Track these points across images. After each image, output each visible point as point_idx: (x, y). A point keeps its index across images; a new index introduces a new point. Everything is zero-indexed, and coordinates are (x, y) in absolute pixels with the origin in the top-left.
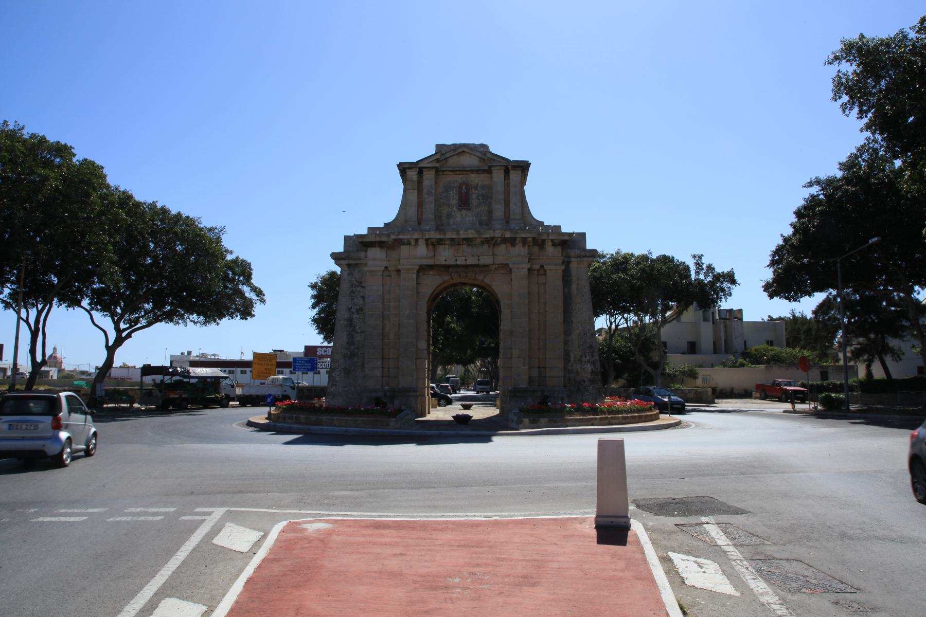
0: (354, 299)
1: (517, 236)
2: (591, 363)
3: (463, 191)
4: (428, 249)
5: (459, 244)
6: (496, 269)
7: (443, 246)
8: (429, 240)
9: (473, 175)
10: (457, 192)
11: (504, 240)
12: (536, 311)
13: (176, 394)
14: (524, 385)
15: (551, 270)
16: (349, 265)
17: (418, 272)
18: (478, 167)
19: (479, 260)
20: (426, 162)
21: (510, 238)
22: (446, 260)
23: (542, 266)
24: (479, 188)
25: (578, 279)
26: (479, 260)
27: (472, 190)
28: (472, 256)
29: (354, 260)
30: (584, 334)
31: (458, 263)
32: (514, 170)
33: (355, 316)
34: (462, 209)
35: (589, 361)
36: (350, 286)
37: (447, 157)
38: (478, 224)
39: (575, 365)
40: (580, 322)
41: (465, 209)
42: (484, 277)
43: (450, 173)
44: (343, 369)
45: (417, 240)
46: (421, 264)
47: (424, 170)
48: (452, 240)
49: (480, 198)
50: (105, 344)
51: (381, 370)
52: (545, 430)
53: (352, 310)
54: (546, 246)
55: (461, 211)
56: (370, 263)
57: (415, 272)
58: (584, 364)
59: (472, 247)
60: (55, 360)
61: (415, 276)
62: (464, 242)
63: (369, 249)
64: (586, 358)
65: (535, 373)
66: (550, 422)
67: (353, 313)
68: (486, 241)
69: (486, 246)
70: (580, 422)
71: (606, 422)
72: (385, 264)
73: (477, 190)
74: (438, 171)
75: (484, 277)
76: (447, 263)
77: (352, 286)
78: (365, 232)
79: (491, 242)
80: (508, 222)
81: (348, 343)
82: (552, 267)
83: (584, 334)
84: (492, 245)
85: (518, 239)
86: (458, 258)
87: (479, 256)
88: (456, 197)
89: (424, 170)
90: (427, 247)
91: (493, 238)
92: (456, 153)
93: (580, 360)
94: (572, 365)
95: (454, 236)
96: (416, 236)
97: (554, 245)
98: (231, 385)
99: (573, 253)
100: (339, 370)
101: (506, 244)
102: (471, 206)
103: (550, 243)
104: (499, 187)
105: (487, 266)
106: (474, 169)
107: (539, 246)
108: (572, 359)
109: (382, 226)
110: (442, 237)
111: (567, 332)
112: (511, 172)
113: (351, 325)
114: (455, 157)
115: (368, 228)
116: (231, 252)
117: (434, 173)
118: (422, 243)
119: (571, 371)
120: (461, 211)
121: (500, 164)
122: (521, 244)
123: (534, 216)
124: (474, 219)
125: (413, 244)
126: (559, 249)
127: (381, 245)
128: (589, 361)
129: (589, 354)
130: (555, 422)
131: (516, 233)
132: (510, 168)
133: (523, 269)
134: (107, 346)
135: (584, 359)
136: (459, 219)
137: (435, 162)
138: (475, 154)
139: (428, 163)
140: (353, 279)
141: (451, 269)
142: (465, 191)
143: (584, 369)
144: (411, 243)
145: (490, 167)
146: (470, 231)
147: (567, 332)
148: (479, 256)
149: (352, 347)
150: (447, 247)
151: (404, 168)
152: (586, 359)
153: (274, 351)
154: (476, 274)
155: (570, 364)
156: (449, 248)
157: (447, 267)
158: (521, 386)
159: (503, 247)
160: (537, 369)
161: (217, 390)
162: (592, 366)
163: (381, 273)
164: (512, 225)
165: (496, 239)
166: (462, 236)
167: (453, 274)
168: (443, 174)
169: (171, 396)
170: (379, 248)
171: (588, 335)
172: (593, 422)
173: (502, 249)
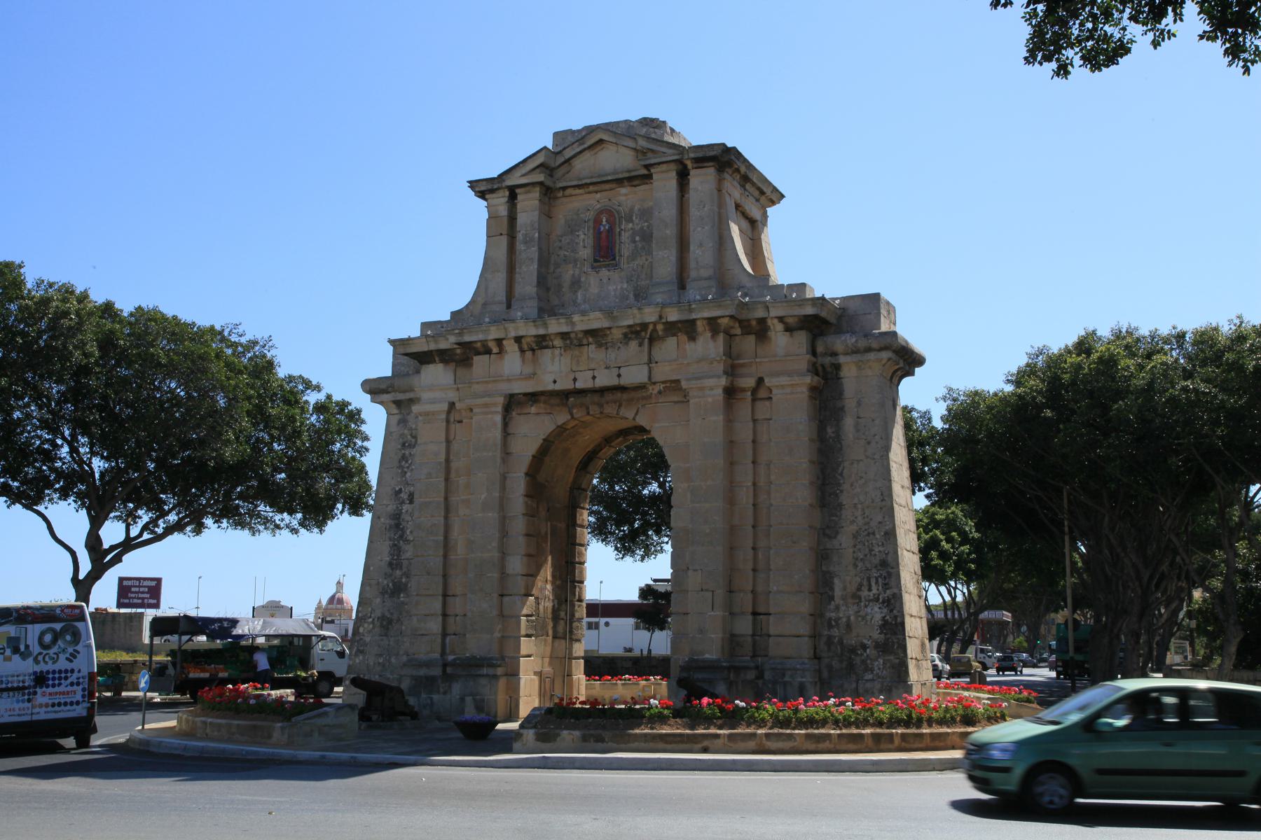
0: (406, 473)
1: (694, 316)
2: (883, 602)
3: (602, 229)
4: (523, 361)
5: (581, 345)
6: (660, 392)
8: (523, 340)
9: (623, 190)
10: (591, 231)
11: (672, 328)
12: (750, 484)
13: (203, 671)
14: (712, 652)
15: (783, 387)
16: (398, 403)
17: (507, 409)
18: (629, 171)
19: (619, 376)
20: (518, 173)
22: (555, 382)
23: (760, 381)
25: (859, 404)
26: (619, 376)
27: (620, 224)
28: (607, 368)
29: (404, 392)
30: (868, 534)
31: (579, 385)
32: (696, 168)
33: (406, 507)
34: (600, 267)
35: (877, 600)
36: (399, 447)
37: (567, 157)
38: (631, 296)
39: (843, 608)
40: (860, 506)
41: (605, 266)
42: (636, 414)
43: (578, 191)
44: (378, 618)
45: (499, 342)
46: (511, 392)
48: (564, 336)
50: (71, 576)
51: (440, 618)
52: (523, 759)
53: (402, 495)
54: (771, 334)
55: (597, 272)
56: (425, 396)
57: (500, 409)
58: (866, 606)
59: (607, 349)
60: (339, 606)
61: (498, 418)
62: (591, 340)
63: (424, 366)
64: (870, 590)
65: (744, 626)
66: (585, 739)
67: (403, 502)
68: (632, 333)
69: (633, 344)
70: (667, 742)
71: (752, 744)
72: (452, 395)
74: (549, 193)
75: (636, 414)
76: (558, 387)
77: (404, 444)
78: (415, 332)
79: (643, 334)
80: (682, 286)
81: (390, 564)
82: (784, 380)
83: (868, 534)
85: (699, 323)
86: (578, 375)
87: (619, 368)
88: (590, 242)
89: (518, 191)
90: (521, 356)
92: (586, 146)
93: (856, 597)
94: (837, 608)
95: (565, 329)
96: (494, 333)
97: (789, 329)
98: (337, 652)
99: (839, 343)
100: (371, 620)
101: (674, 335)
102: (617, 258)
103: (780, 327)
104: (669, 212)
105: (641, 387)
106: (620, 176)
108: (838, 592)
110: (541, 332)
111: (827, 530)
112: (692, 172)
113: (397, 526)
114: (587, 155)
116: (318, 388)
117: (538, 194)
119: (833, 623)
121: (664, 159)
122: (709, 334)
125: (495, 350)
126: (802, 338)
127: (444, 356)
128: (877, 600)
129: (877, 583)
130: (600, 739)
131: (691, 311)
132: (689, 164)
133: (711, 389)
134: (75, 580)
135: (864, 593)
136: (594, 290)
137: (538, 170)
138: (625, 144)
140: (406, 432)
141: (572, 399)
143: (864, 618)
145: (647, 167)
146: (592, 315)
147: (827, 530)
148: (619, 368)
149: (398, 573)
150: (557, 352)
151: (483, 189)
152: (871, 594)
153: (655, 581)
154: (620, 406)
155: (832, 606)
156: (561, 355)
157: (564, 395)
158: (707, 656)
159: (671, 342)
160: (750, 617)
161: (305, 664)
162: (885, 610)
163: (444, 416)
164: (693, 293)
165: (651, 327)
166: (581, 327)
167: (575, 411)
168: (564, 196)
169: (192, 675)
170: (441, 364)
171: (878, 536)
172: (706, 743)
173: (670, 346)
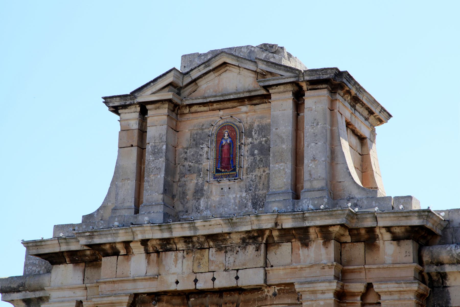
1: (307, 224)
3: (224, 142)
4: (148, 263)
5: (202, 249)
6: (275, 295)
7: (173, 253)
8: (149, 243)
9: (244, 109)
15: (391, 293)
20: (149, 91)
21: (294, 229)
22: (177, 282)
23: (369, 286)
24: (253, 133)
26: (237, 278)
28: (225, 270)
29: (34, 291)
31: (200, 286)
32: (310, 90)
38: (250, 204)
43: (203, 108)
45: (127, 244)
46: (136, 292)
47: (148, 107)
48: (187, 239)
49: (256, 152)
54: (380, 242)
59: (226, 252)
62: (211, 244)
68: (250, 238)
69: (251, 249)
72: (80, 295)
73: (251, 136)
76: (180, 287)
79: (260, 239)
82: (392, 287)
84: (263, 246)
85: (312, 231)
86: (199, 276)
87: (237, 270)
88: (212, 154)
89: (148, 107)
91: (261, 232)
92: (211, 68)
95: (188, 233)
97: (396, 238)
105: (257, 289)
107: (364, 241)
109: (79, 221)
110: (166, 235)
112: (307, 93)
114: (212, 76)
115: (55, 226)
118: (137, 249)
120: (219, 182)
122: (321, 241)
123: (106, 193)
124: (244, 195)
125: (123, 252)
131: (304, 219)
132: (305, 86)
133: (323, 292)
136: (215, 198)
139: (154, 93)
142: (228, 141)
144: (119, 252)
145: (266, 88)
148: (237, 270)
150: (180, 254)
156: (184, 257)
159: (286, 247)
166: (202, 231)
